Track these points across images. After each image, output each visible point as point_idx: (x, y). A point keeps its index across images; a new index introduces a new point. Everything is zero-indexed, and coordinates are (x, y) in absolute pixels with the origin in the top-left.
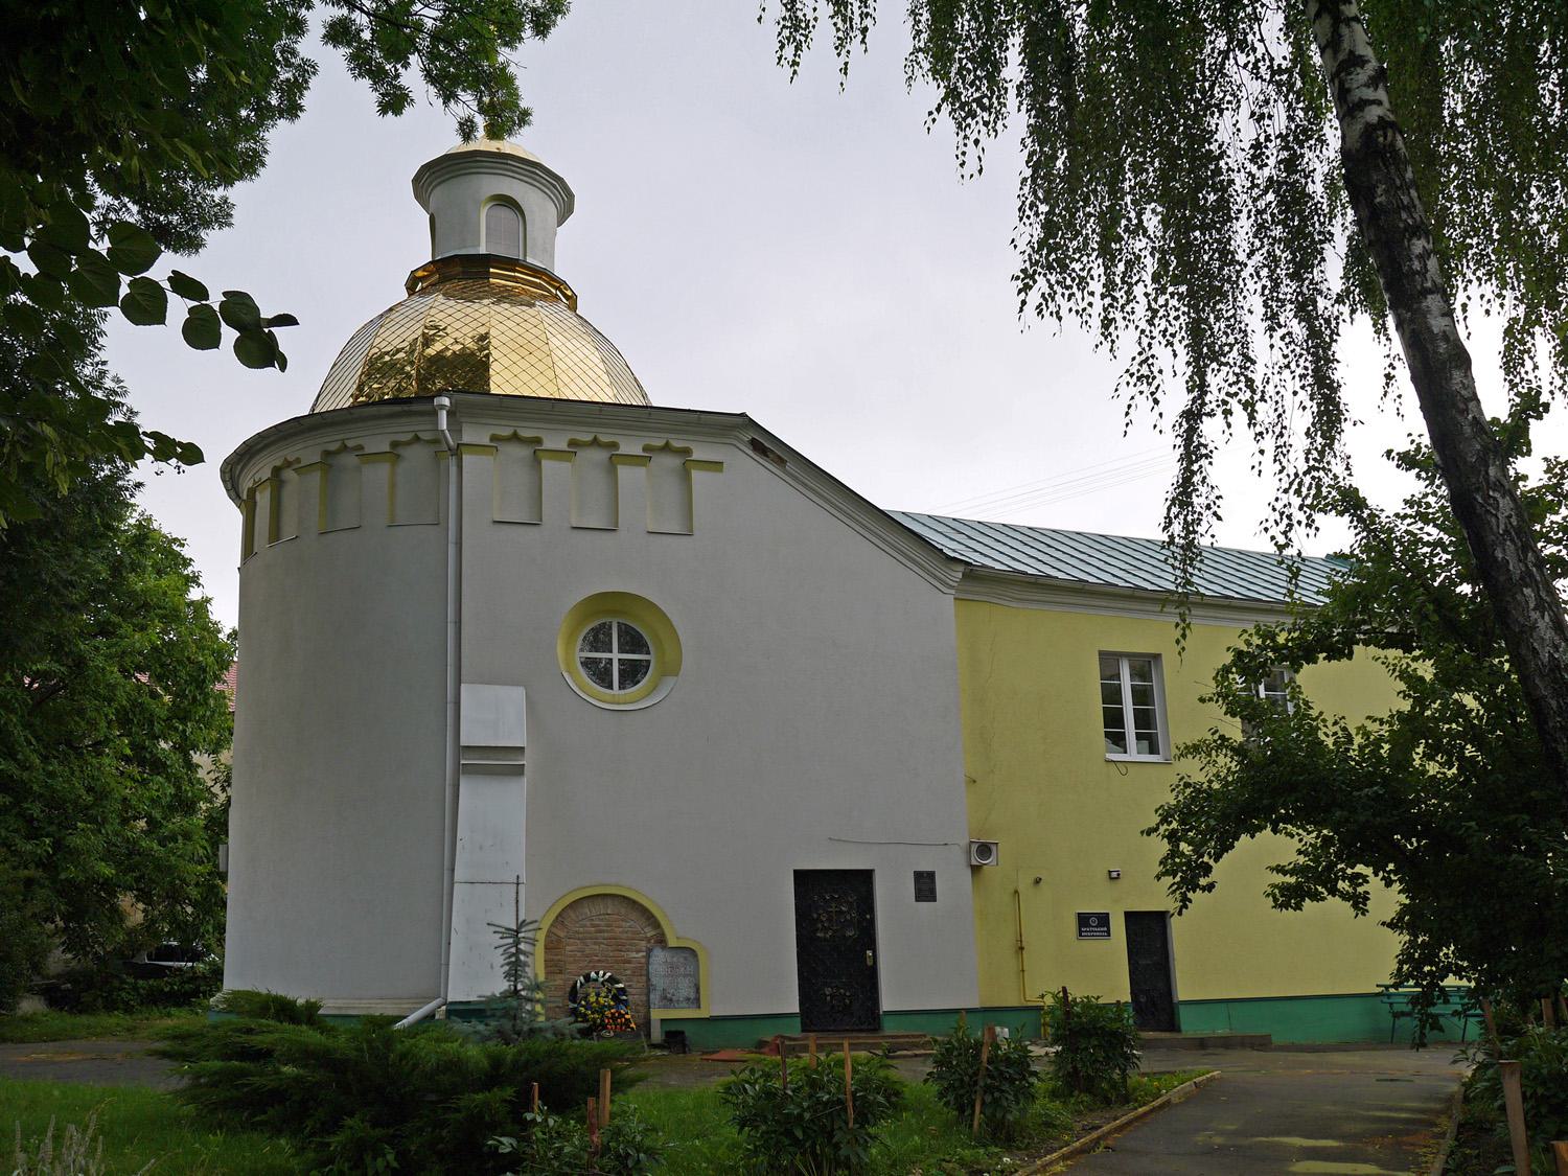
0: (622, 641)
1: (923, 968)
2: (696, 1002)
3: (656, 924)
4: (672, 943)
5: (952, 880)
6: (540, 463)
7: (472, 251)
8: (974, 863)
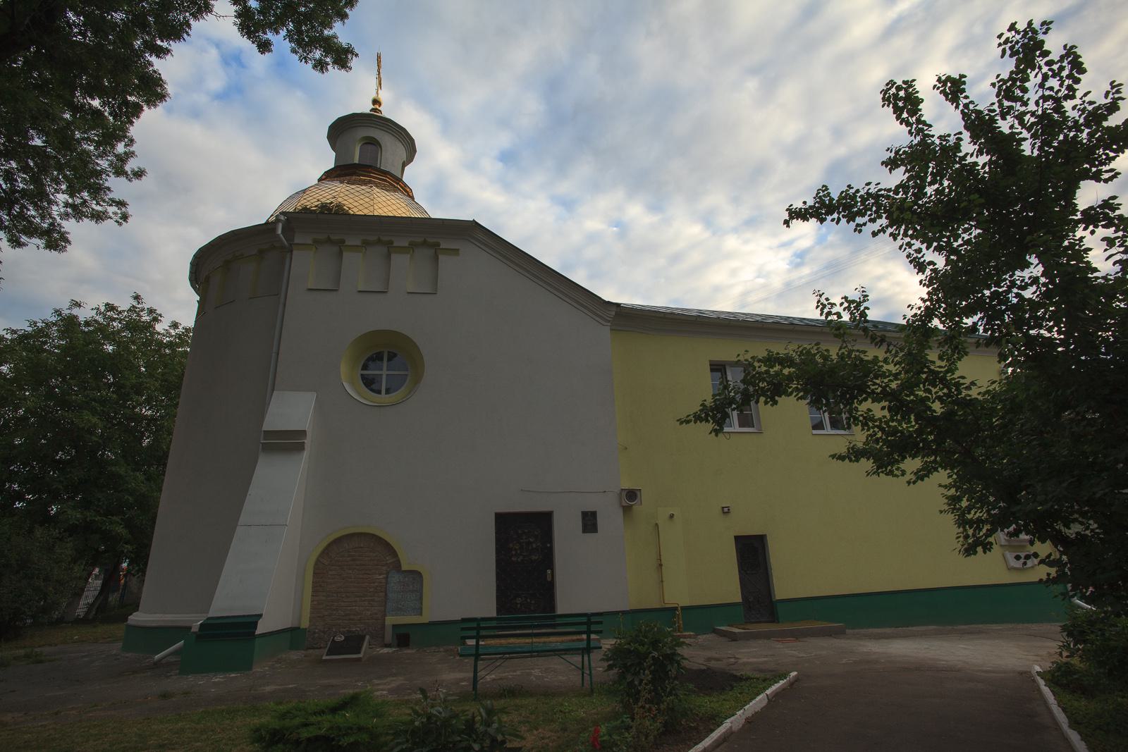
0: (387, 360)
1: (590, 579)
2: (419, 611)
3: (393, 553)
4: (405, 567)
5: (610, 518)
6: (438, 259)
7: (351, 162)
8: (624, 504)
